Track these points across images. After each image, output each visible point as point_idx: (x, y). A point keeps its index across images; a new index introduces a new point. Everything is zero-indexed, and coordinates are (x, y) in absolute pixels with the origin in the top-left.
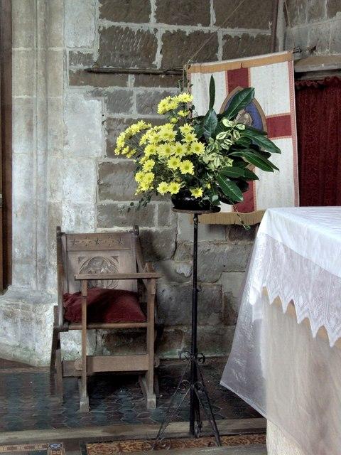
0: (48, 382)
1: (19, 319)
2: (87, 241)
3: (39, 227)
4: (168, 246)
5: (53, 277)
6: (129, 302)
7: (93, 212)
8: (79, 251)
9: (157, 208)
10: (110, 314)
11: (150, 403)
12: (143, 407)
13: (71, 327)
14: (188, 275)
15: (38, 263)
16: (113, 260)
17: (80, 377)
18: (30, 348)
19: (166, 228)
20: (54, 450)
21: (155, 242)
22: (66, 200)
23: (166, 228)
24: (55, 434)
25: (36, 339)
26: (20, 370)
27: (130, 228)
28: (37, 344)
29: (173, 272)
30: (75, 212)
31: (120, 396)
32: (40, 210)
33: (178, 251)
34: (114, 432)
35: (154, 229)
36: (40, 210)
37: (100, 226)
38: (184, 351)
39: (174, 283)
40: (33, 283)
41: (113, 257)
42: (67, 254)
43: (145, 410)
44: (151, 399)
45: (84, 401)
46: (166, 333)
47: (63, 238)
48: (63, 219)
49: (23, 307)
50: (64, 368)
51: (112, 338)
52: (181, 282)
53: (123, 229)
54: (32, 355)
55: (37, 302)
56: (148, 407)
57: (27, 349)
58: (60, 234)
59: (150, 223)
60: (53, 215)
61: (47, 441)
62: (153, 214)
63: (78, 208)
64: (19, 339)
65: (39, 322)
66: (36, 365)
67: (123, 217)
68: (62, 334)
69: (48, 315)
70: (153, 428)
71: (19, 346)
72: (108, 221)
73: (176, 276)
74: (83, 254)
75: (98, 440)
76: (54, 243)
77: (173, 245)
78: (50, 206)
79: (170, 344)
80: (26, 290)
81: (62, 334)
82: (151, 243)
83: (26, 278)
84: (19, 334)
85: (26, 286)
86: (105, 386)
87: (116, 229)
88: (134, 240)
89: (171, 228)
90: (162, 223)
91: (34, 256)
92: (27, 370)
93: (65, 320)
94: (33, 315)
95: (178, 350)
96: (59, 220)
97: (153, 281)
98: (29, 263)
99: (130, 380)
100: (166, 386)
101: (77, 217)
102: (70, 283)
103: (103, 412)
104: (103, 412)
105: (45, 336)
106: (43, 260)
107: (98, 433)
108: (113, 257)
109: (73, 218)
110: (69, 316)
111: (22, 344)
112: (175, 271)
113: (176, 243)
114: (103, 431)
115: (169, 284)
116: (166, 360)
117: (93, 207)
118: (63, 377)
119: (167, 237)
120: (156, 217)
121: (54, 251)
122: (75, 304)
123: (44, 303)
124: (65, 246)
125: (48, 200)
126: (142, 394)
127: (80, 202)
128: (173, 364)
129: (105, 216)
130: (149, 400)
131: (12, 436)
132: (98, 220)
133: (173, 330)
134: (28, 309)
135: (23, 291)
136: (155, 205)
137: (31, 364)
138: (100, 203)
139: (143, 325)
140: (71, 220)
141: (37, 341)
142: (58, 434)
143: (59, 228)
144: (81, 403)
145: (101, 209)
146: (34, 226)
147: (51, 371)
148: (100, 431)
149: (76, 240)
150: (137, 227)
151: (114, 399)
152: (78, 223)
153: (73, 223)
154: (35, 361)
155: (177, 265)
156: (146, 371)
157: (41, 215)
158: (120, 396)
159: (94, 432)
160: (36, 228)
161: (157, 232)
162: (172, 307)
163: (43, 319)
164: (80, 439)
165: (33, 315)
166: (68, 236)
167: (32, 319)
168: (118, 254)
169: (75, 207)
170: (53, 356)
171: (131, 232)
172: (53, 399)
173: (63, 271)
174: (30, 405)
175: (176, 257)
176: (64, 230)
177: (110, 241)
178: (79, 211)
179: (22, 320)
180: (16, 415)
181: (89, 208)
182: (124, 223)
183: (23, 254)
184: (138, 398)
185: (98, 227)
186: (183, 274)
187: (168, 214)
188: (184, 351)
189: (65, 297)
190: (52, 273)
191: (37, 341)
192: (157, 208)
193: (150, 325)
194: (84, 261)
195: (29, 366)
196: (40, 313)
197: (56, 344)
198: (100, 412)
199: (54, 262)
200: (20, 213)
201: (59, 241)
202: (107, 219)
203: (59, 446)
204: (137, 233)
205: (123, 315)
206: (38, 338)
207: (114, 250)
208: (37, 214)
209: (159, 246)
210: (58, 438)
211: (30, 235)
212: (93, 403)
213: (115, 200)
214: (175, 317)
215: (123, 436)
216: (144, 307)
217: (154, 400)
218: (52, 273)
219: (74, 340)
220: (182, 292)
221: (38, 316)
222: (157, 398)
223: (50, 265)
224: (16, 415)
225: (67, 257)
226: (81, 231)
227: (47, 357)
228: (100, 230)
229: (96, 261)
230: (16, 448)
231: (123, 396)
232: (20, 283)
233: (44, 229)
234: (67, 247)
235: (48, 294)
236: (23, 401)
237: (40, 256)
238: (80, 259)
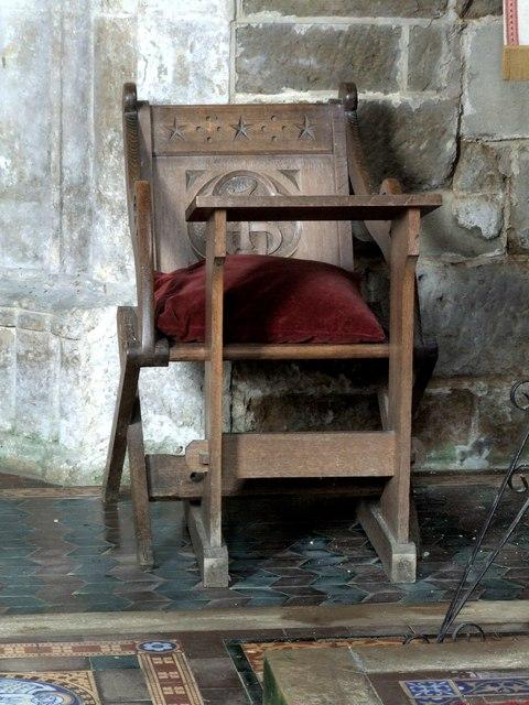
0: (97, 517)
1: (12, 356)
2: (210, 126)
3: (69, 93)
4: (436, 147)
5: (114, 235)
6: (339, 289)
7: (224, 47)
8: (188, 154)
9: (405, 38)
10: (282, 320)
11: (401, 565)
12: (382, 578)
13: (174, 352)
14: (492, 232)
15: (67, 198)
16: (283, 180)
17: (196, 502)
18: (45, 435)
19: (431, 96)
20: (153, 654)
21: (398, 136)
22: (149, 11)
23: (431, 96)
24: (149, 621)
25: (61, 409)
26: (20, 494)
27: (327, 95)
28: (63, 422)
29: (448, 222)
30: (174, 45)
31: (312, 554)
32: (72, 44)
33: (462, 165)
34: (316, 620)
35: (395, 99)
36: (72, 44)
37: (242, 87)
38: (478, 447)
39: (449, 256)
40: (51, 256)
41: (283, 172)
42: (155, 161)
43: (386, 586)
44: (405, 554)
45: (215, 558)
46: (430, 397)
47: (144, 117)
48: (141, 65)
49: (25, 322)
50: (153, 474)
51: (274, 411)
52: (473, 254)
53: (308, 97)
54: (48, 455)
55: (63, 306)
56: (394, 577)
57: (34, 438)
58: (133, 106)
59: (386, 80)
60: (111, 55)
61: (130, 636)
62: (395, 55)
63: (183, 34)
64: (13, 416)
65: (69, 362)
66: (61, 482)
67: (311, 62)
68: (146, 374)
69: (99, 347)
70: (423, 613)
71: (12, 433)
72: (267, 73)
73: (458, 234)
74: (198, 163)
75: (275, 637)
76: (115, 136)
77: (450, 145)
78: (101, 30)
79: (438, 430)
80: (31, 274)
81: (146, 374)
82: (388, 140)
83: (29, 242)
84: (13, 398)
85: (29, 265)
86: (280, 522)
87: (289, 96)
88: (342, 126)
89: (445, 97)
90: (421, 81)
91: (55, 175)
92: (50, 492)
93: (159, 334)
94: (54, 343)
95: (459, 449)
96: (128, 69)
97: (414, 216)
98: (37, 199)
99: (339, 506)
100: (438, 532)
101: (180, 61)
102: (162, 242)
103: (268, 588)
104: (268, 588)
105: (88, 400)
106: (80, 189)
107: (271, 620)
108: (283, 172)
109: (170, 63)
110: (167, 322)
111: (20, 426)
112: (456, 220)
113: (458, 139)
114: (284, 618)
115: (437, 257)
116: (427, 474)
117: (225, 30)
118: (152, 499)
119: (433, 120)
120: (403, 64)
121: (116, 161)
122: (183, 292)
123: (84, 307)
124: (147, 139)
125: (96, 13)
126: (378, 549)
127: (188, 18)
128: (448, 484)
129: (259, 59)
130: (396, 557)
131: (31, 625)
132: (238, 70)
133: (447, 391)
134: (38, 325)
135: (21, 277)
136: (399, 28)
137: (49, 478)
138: (244, 20)
139: (377, 350)
140: (162, 70)
141: (64, 415)
142: (157, 621)
143: (131, 88)
144: (207, 562)
145: (249, 40)
146: (54, 90)
147: (107, 496)
148: (278, 616)
149: (181, 122)
150: (351, 88)
151: (293, 561)
152: (182, 78)
153: (169, 78)
154: (60, 469)
155: (462, 205)
156: (388, 479)
157: (74, 58)
158: (312, 554)
159: (258, 618)
160: (61, 95)
161: (404, 106)
162: (444, 324)
163: (82, 351)
164: (223, 632)
165: (54, 343)
166: (157, 112)
167: (49, 354)
168: (298, 164)
169: (174, 32)
170: (119, 445)
171: (333, 102)
172: (121, 559)
173: (146, 204)
174: (61, 568)
175: (458, 182)
176: (142, 96)
177: (275, 127)
178: (183, 44)
179: (19, 358)
180: (25, 591)
181: (211, 34)
182: (311, 81)
183: (21, 175)
184: (361, 560)
185: (237, 91)
186: (477, 229)
187: (439, 54)
188: (478, 447)
189: (152, 278)
190: (107, 223)
191: (64, 415)
192: (405, 38)
193: (401, 353)
194: (202, 181)
195: (44, 485)
196: (74, 334)
197: (129, 409)
198: (263, 583)
199: (115, 189)
200: (14, 55)
201: (132, 126)
202: (267, 65)
203: (167, 646)
204: (353, 104)
205: (321, 322)
206: (68, 407)
207: (287, 152)
208: (63, 54)
209: (411, 147)
210: (162, 630)
211: (41, 119)
212: (239, 568)
213: (286, 13)
214: (454, 355)
215: (343, 629)
216: (381, 308)
217: (412, 557)
218: (107, 223)
219: (170, 413)
220: (472, 282)
221: (68, 345)
222: (419, 559)
223: (101, 199)
224: (25, 591)
225: (155, 169)
226: (191, 99)
227: (96, 458)
228: (243, 98)
229: (235, 184)
230: (48, 650)
231: (319, 554)
232: (14, 255)
233: (84, 98)
234: (153, 147)
235: (96, 283)
236: (39, 562)
237: (72, 175)
238: (189, 177)
